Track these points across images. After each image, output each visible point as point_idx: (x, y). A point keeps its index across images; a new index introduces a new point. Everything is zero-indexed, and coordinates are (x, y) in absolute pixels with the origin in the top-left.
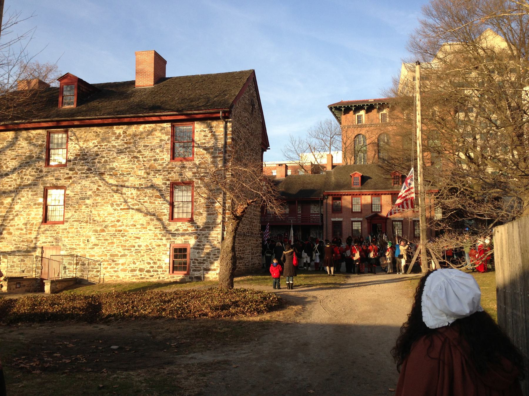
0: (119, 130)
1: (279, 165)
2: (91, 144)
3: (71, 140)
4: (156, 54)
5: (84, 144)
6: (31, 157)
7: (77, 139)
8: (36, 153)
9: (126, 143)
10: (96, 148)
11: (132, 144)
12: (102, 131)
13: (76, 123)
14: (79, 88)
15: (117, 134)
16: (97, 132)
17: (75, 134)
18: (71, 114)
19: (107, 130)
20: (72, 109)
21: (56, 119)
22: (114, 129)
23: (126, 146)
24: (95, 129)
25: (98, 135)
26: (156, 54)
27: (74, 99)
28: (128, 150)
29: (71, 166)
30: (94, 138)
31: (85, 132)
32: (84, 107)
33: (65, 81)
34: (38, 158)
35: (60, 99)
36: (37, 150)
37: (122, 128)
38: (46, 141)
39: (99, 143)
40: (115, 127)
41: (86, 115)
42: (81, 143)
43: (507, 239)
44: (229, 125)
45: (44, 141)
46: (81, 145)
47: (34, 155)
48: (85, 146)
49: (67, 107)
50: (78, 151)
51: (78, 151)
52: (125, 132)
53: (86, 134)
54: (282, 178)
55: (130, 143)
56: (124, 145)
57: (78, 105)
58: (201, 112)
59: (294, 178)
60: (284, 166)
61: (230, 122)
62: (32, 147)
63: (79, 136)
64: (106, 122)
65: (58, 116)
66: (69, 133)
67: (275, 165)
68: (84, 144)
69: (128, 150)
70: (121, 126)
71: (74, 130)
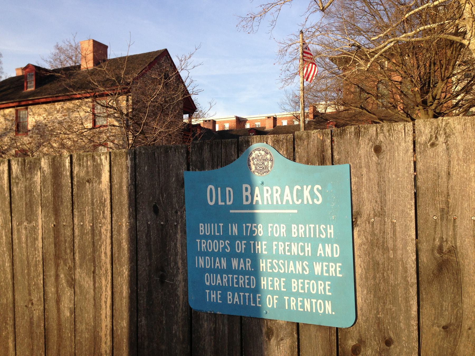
0: (58, 106)
1: (268, 118)
2: (42, 118)
3: (30, 115)
4: (94, 41)
5: (37, 117)
6: (6, 129)
7: (34, 114)
8: (9, 125)
9: (64, 115)
10: (46, 121)
11: (68, 116)
12: (49, 107)
13: (30, 102)
14: (36, 74)
15: (58, 109)
16: (45, 108)
17: (32, 111)
18: (32, 94)
19: (52, 106)
20: (32, 91)
21: (18, 100)
22: (56, 105)
23: (63, 118)
24: (45, 106)
25: (46, 110)
26: (94, 41)
27: (33, 83)
28: (65, 120)
29: (31, 135)
30: (44, 112)
31: (38, 109)
32: (38, 90)
33: (27, 70)
34: (10, 129)
35: (25, 84)
36: (10, 123)
37: (61, 104)
38: (15, 116)
39: (47, 116)
40: (56, 103)
41: (36, 96)
42: (36, 117)
43: (133, 194)
44: (130, 97)
45: (13, 117)
46: (36, 119)
47: (8, 127)
48: (38, 119)
49: (29, 90)
50: (34, 123)
51: (34, 123)
52: (62, 107)
53: (38, 110)
54: (270, 129)
55: (66, 115)
56: (62, 117)
57: (36, 88)
58: (383, 50)
59: (281, 129)
60: (272, 118)
61: (130, 95)
62: (7, 122)
63: (34, 112)
64: (48, 100)
65: (19, 98)
66: (29, 110)
67: (264, 118)
68: (37, 117)
69: (65, 120)
70: (60, 103)
71: (31, 107)
